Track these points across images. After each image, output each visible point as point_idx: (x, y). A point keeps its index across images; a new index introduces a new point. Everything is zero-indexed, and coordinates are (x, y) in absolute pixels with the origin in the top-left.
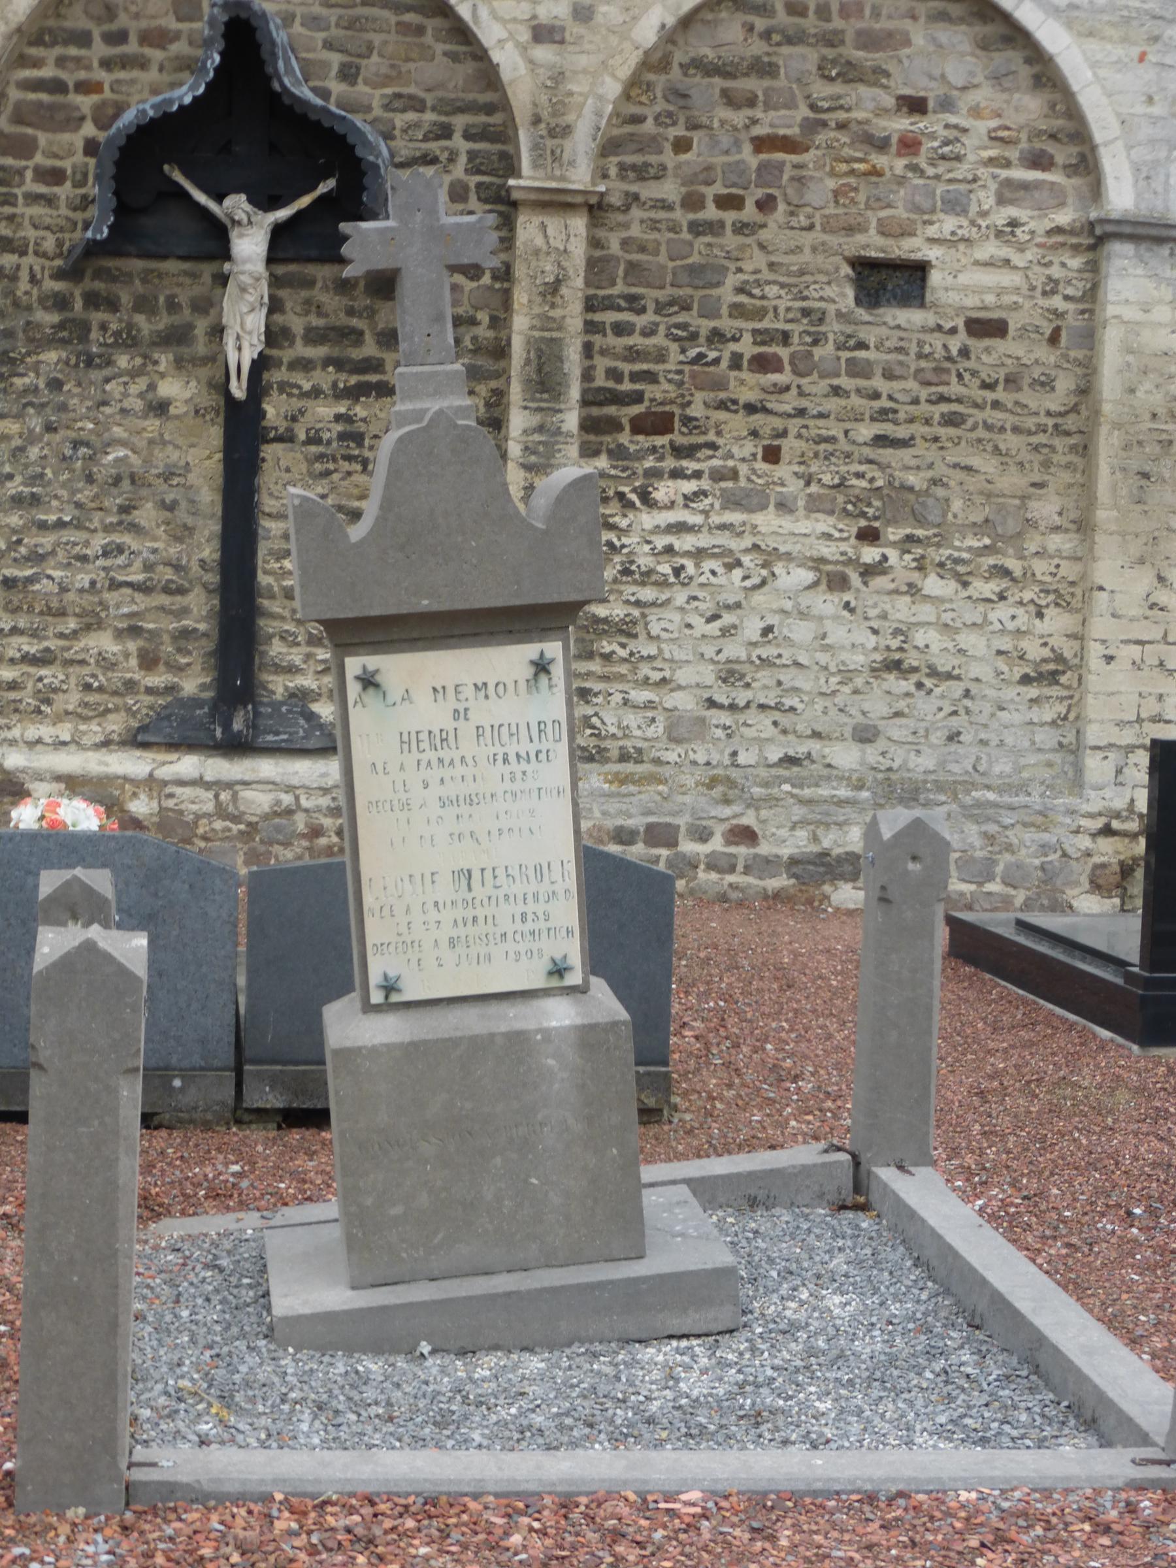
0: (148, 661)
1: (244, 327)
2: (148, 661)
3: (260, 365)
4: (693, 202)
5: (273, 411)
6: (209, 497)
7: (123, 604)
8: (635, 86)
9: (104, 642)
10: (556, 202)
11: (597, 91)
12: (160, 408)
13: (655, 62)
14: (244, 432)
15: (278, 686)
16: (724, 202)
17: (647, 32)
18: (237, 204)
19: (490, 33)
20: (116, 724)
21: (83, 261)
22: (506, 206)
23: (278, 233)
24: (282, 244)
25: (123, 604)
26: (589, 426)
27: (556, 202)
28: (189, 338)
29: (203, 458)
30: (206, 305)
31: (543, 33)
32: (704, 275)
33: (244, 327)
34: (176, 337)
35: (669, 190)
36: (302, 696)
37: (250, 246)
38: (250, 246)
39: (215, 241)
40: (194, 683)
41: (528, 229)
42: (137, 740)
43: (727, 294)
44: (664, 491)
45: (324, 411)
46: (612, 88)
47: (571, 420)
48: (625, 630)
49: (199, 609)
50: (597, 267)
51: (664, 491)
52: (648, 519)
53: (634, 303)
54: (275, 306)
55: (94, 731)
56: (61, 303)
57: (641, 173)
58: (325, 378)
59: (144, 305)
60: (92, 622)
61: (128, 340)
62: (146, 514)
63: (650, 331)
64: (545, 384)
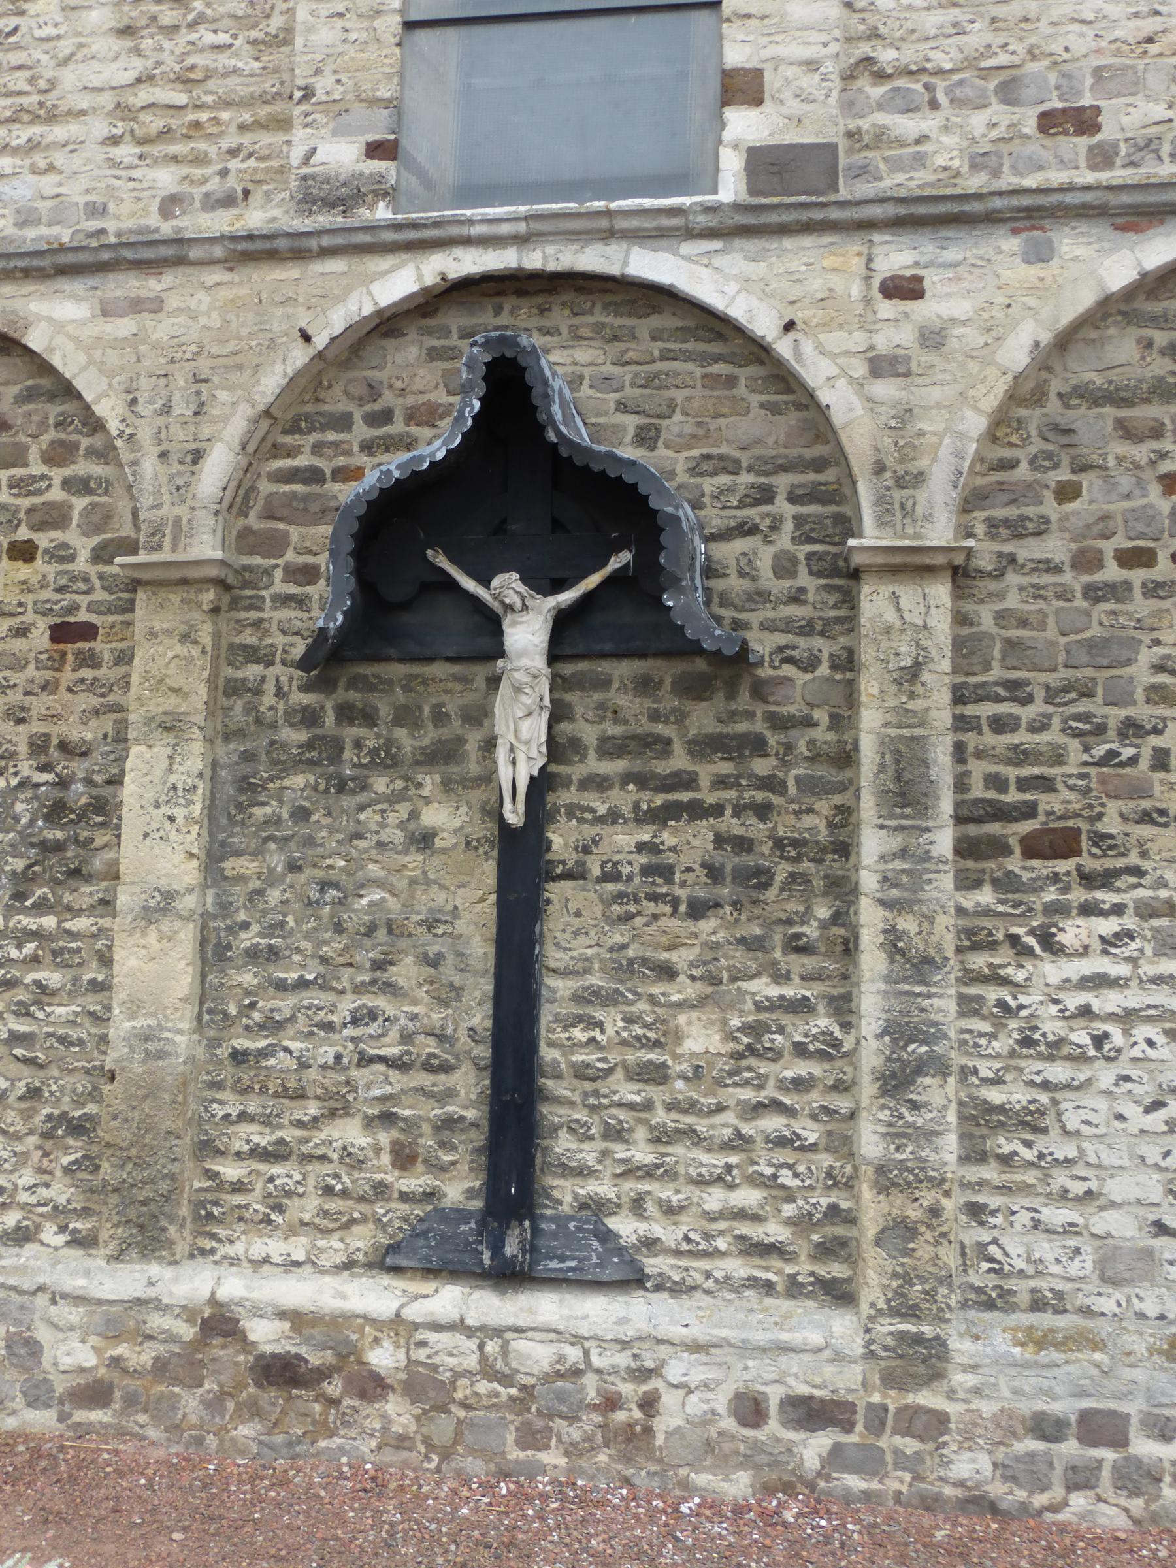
0: (404, 1159)
1: (520, 735)
2: (404, 1159)
3: (541, 785)
4: (1086, 561)
5: (561, 840)
6: (480, 949)
7: (375, 1084)
8: (1002, 424)
9: (349, 1132)
10: (910, 565)
11: (955, 426)
12: (424, 840)
13: (1025, 393)
14: (522, 865)
15: (565, 1193)
16: (1133, 558)
17: (1016, 354)
18: (508, 585)
19: (816, 371)
20: (362, 1240)
21: (327, 659)
22: (846, 576)
23: (563, 623)
24: (566, 635)
25: (375, 1084)
26: (965, 849)
27: (910, 565)
28: (455, 758)
29: (470, 902)
30: (479, 715)
31: (883, 366)
32: (1109, 651)
33: (520, 735)
34: (443, 755)
35: (1055, 547)
36: (595, 1208)
37: (527, 636)
38: (527, 636)
39: (485, 633)
40: (460, 1188)
41: (875, 602)
42: (387, 1261)
43: (1141, 673)
44: (1072, 932)
45: (623, 840)
46: (975, 424)
47: (943, 841)
48: (1030, 1122)
49: (468, 1092)
50: (966, 648)
51: (1072, 932)
52: (1053, 971)
53: (1017, 691)
54: (558, 713)
55: (335, 1248)
56: (309, 717)
57: (1018, 529)
58: (624, 798)
59: (405, 717)
60: (337, 1107)
61: (386, 759)
62: (405, 972)
63: (1040, 725)
64: (906, 795)
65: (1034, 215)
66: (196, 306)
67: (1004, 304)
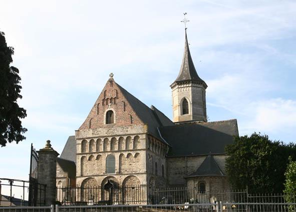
11: (122, 181)
65: (124, 174)
66: (100, 177)
67: (124, 177)
